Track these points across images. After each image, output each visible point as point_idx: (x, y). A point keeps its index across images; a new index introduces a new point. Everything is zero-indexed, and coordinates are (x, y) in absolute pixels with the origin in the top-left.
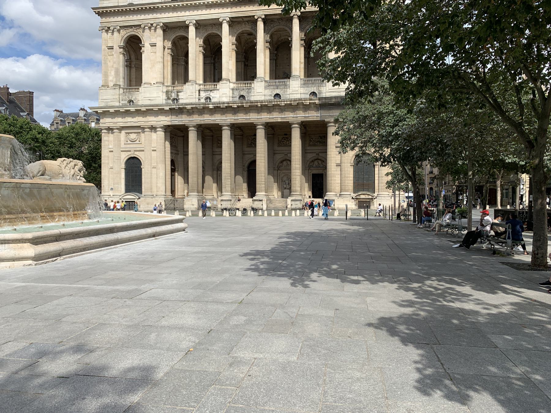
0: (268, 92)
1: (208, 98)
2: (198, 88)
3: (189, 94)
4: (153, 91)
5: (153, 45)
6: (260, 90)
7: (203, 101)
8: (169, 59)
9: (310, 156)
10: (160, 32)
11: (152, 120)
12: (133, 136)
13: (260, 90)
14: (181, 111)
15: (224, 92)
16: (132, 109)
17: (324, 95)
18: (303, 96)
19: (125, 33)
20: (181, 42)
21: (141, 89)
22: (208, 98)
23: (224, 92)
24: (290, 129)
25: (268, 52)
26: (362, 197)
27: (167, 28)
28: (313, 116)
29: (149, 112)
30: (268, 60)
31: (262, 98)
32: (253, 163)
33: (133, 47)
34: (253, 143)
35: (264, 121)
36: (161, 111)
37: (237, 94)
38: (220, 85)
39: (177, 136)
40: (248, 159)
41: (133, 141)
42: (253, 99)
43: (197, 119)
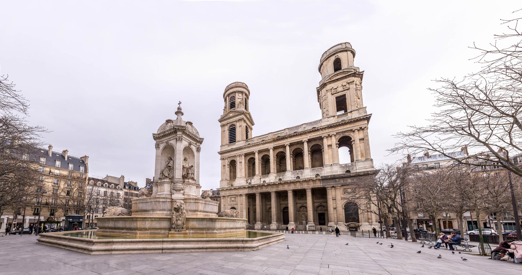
0: (293, 176)
1: (264, 181)
2: (259, 177)
3: (256, 181)
4: (241, 181)
5: (241, 163)
6: (289, 176)
7: (262, 182)
8: (247, 167)
9: (316, 204)
10: (243, 157)
11: (242, 192)
12: (233, 199)
13: (289, 176)
14: (252, 187)
15: (272, 178)
16: (233, 188)
17: (323, 175)
18: (312, 176)
19: (230, 160)
20: (252, 160)
21: (236, 180)
22: (264, 181)
23: (272, 178)
24: (287, 193)
25: (292, 159)
26: (351, 225)
27: (246, 155)
28: (319, 185)
29: (240, 188)
30: (292, 162)
31: (291, 179)
32: (287, 208)
33: (233, 164)
34: (270, 200)
35: (292, 189)
36: (244, 188)
37: (278, 178)
38: (255, 177)
39: (251, 197)
40: (283, 206)
41: (233, 201)
42: (285, 180)
43: (260, 190)
